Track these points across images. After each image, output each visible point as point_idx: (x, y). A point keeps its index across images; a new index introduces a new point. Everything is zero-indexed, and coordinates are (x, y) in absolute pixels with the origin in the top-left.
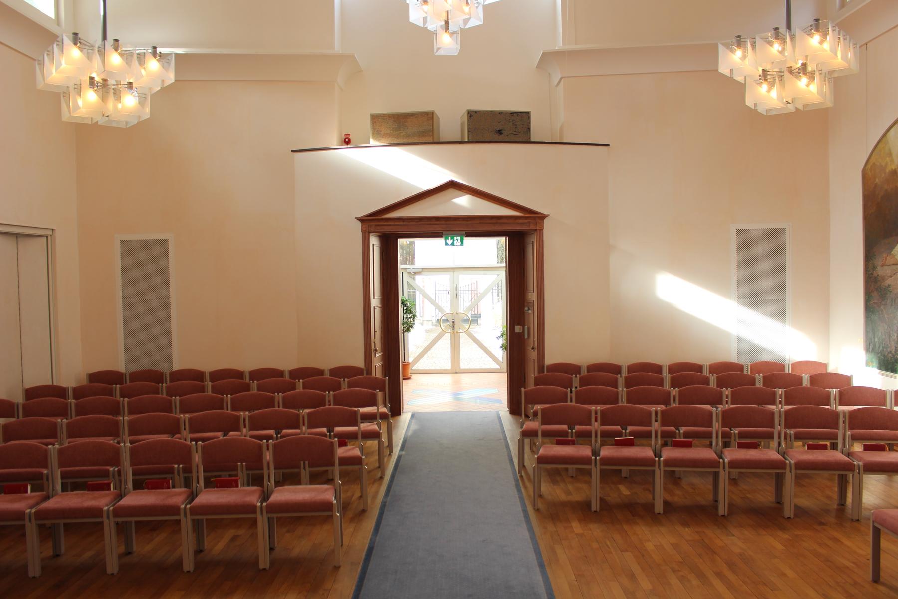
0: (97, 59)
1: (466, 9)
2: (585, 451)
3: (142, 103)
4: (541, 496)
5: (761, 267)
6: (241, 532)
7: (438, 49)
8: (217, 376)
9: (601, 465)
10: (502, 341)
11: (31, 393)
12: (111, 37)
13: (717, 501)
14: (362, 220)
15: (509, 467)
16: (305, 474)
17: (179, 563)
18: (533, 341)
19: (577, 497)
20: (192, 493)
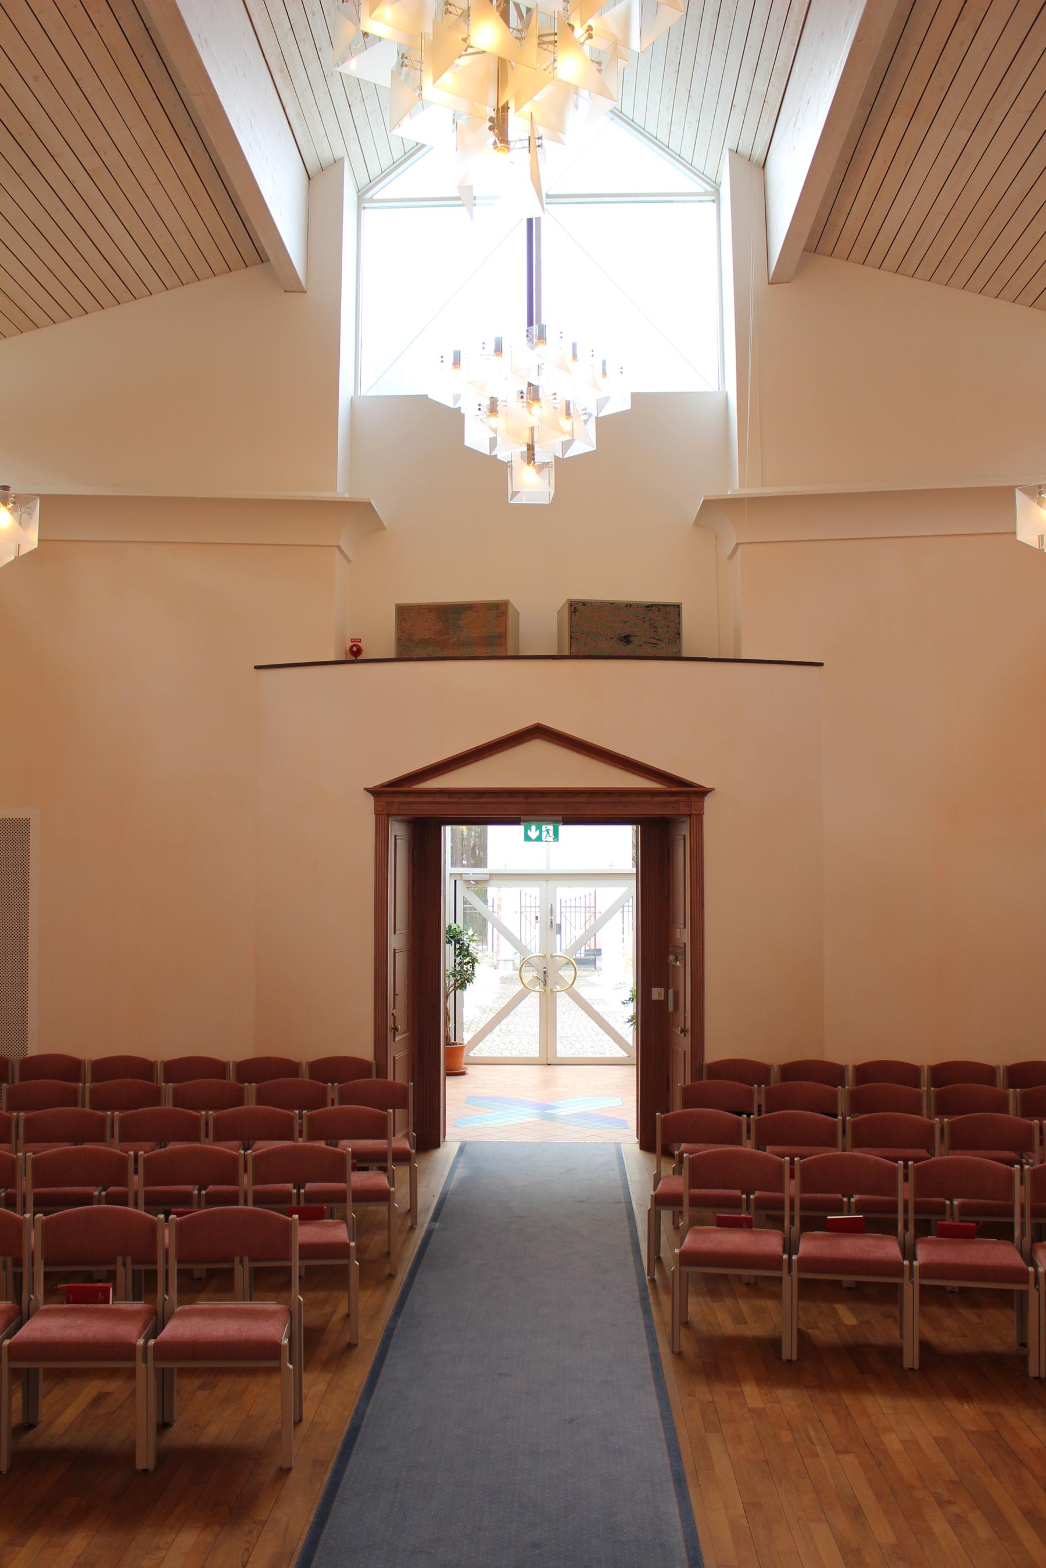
1: (566, 424)
2: (769, 1242)
4: (686, 1324)
6: (113, 1386)
7: (515, 494)
9: (800, 1270)
10: (630, 1010)
13: (1024, 1345)
14: (376, 792)
15: (631, 1260)
16: (242, 1272)
18: (684, 1016)
19: (754, 1329)
20: (20, 1313)
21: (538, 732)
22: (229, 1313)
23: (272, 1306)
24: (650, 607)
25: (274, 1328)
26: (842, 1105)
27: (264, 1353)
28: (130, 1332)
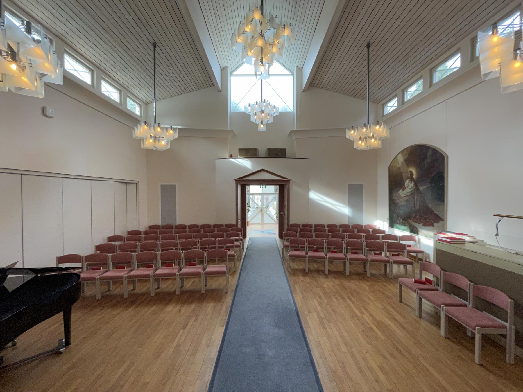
0: (152, 128)
3: (167, 144)
5: (355, 194)
6: (196, 279)
8: (190, 227)
11: (129, 233)
12: (157, 123)
16: (217, 260)
17: (175, 292)
19: (301, 267)
21: (263, 170)
22: (216, 267)
23: (223, 265)
24: (281, 149)
25: (224, 269)
26: (139, 249)
27: (223, 273)
28: (200, 270)
